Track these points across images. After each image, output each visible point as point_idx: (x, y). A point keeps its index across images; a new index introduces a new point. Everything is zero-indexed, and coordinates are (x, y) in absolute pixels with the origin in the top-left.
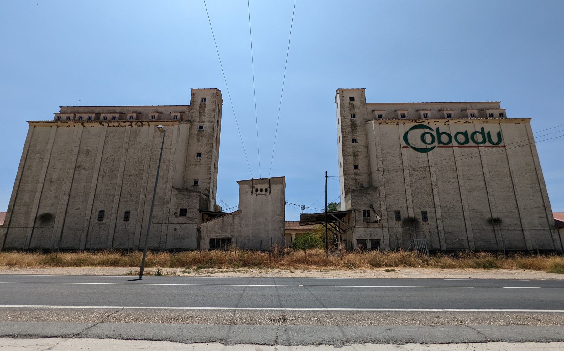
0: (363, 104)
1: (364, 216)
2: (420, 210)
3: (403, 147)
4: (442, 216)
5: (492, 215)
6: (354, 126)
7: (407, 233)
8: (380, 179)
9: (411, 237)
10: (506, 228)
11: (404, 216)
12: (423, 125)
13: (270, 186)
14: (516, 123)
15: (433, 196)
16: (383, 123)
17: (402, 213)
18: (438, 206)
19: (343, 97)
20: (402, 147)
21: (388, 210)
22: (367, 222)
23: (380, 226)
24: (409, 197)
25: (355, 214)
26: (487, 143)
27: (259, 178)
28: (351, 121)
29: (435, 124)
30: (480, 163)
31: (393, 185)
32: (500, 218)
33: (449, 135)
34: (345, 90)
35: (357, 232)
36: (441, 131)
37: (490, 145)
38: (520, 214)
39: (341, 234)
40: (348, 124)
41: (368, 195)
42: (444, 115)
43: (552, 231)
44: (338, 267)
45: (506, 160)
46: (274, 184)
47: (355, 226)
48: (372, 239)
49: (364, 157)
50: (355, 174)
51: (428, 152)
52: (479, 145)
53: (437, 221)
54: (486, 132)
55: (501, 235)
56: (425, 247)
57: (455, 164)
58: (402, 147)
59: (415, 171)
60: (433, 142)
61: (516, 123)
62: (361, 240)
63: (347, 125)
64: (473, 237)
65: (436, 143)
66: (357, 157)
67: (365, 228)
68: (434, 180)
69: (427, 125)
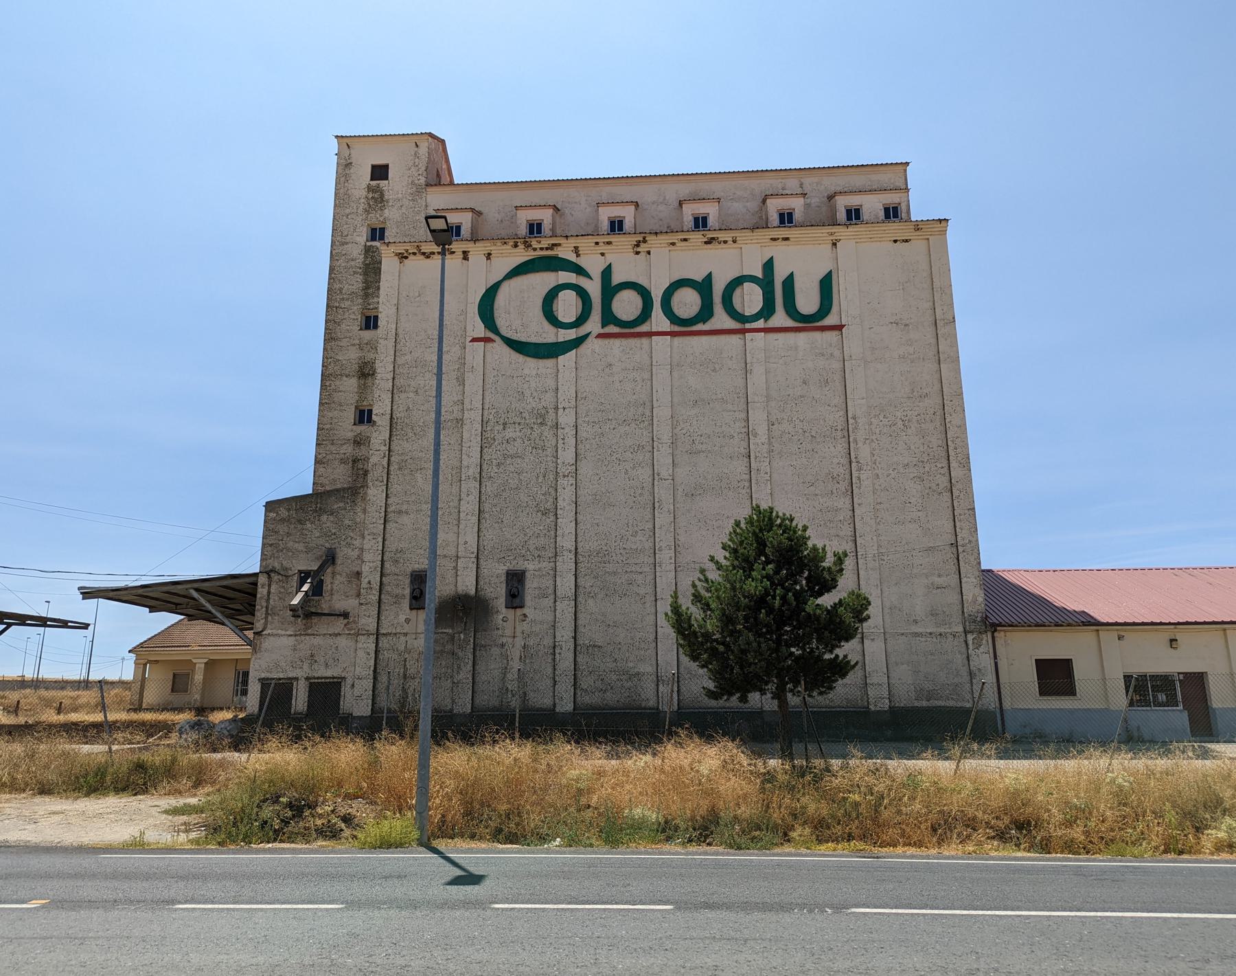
2: (502, 569)
7: (442, 652)
11: (441, 588)
12: (556, 258)
14: (895, 241)
16: (414, 254)
25: (269, 586)
28: (368, 250)
29: (603, 254)
31: (420, 480)
33: (645, 293)
40: (353, 263)
41: (324, 518)
43: (970, 637)
47: (262, 631)
48: (316, 676)
50: (355, 441)
61: (895, 241)
65: (594, 325)
67: (298, 638)
69: (572, 257)
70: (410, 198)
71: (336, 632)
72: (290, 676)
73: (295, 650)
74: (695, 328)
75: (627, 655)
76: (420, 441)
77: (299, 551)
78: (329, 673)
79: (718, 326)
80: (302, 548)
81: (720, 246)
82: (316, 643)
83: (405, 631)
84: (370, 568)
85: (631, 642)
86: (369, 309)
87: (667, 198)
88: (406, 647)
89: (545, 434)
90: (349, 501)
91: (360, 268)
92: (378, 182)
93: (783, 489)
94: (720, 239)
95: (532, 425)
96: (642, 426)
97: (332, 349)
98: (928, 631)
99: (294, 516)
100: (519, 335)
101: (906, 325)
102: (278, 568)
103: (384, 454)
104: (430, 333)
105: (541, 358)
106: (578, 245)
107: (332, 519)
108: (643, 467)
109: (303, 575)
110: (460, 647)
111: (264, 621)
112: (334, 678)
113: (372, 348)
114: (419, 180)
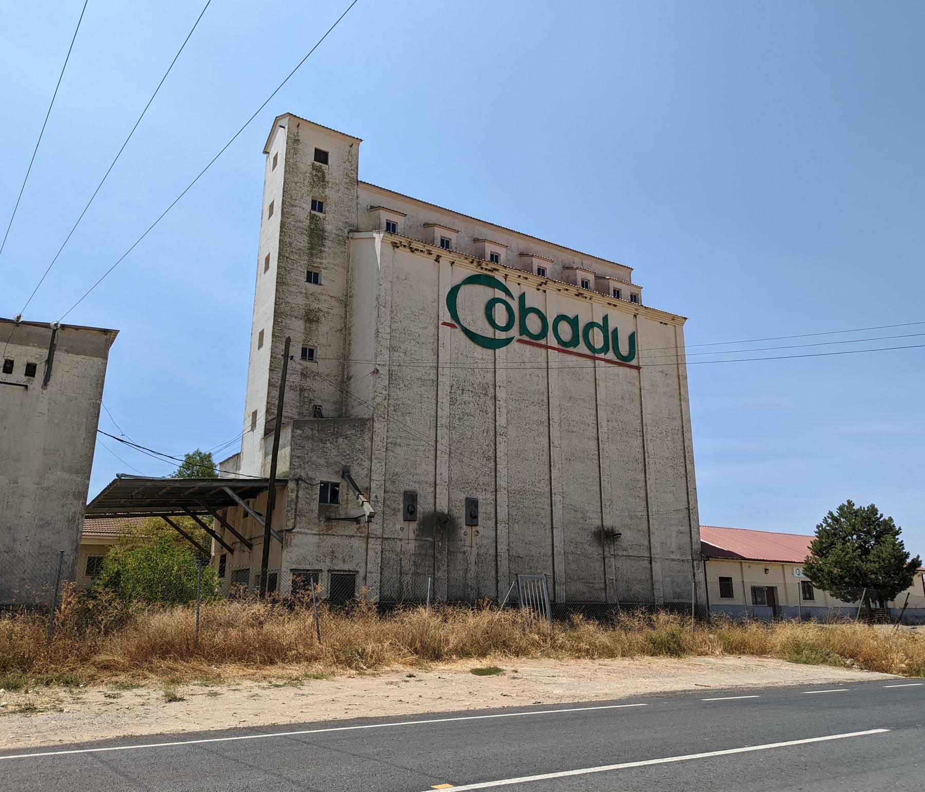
0: (348, 180)
1: (323, 499)
2: (463, 496)
3: (444, 324)
4: (509, 514)
5: (602, 522)
6: (316, 234)
7: (426, 555)
8: (378, 400)
9: (436, 566)
10: (625, 553)
11: (424, 507)
12: (493, 278)
13: (51, 355)
14: (661, 323)
15: (496, 461)
16: (405, 246)
17: (420, 500)
18: (502, 489)
19: (297, 141)
20: (441, 322)
21: (390, 487)
22: (329, 519)
23: (361, 533)
24: (443, 458)
25: (298, 491)
26: (611, 355)
27: (12, 317)
28: (312, 218)
29: (519, 284)
30: (594, 397)
31: (408, 421)
32: (617, 529)
33: (543, 318)
34: (306, 123)
35: (296, 545)
36: (528, 304)
37: (614, 358)
38: (650, 523)
39: (225, 551)
40: (300, 224)
41: (340, 440)
42: (532, 267)
43: (695, 563)
44: (318, 667)
45: (638, 398)
46: (67, 351)
47: (293, 529)
48: (336, 569)
49: (335, 329)
50: (302, 374)
51: (497, 350)
52: (596, 355)
53: (496, 527)
54: (611, 328)
55: (614, 568)
56: (543, 595)
57: (547, 390)
58: (441, 322)
59: (463, 390)
60: (508, 327)
61: (661, 323)
62: (304, 570)
63: (299, 227)
64: (564, 571)
65: (514, 332)
66: (314, 326)
67: (321, 537)
68: (502, 420)
69: (503, 281)
70: (346, 186)
71: (351, 534)
72: (316, 568)
73: (319, 547)
74: (569, 349)
75: (537, 564)
76: (408, 391)
77: (321, 466)
78: (346, 568)
79: (581, 351)
80: (324, 463)
81: (583, 299)
82: (335, 542)
83: (400, 537)
84: (377, 485)
85: (538, 555)
86: (313, 266)
87: (512, 247)
88: (401, 550)
89: (488, 402)
90: (359, 430)
91: (306, 230)
92: (321, 164)
93: (614, 463)
94: (584, 295)
95: (480, 395)
96: (542, 408)
97: (283, 292)
98: (678, 558)
99: (317, 435)
100: (471, 327)
101: (666, 375)
102: (304, 477)
103: (385, 397)
104: (414, 310)
105: (484, 347)
106: (508, 274)
107: (346, 442)
108: (543, 436)
109: (322, 485)
110: (439, 552)
111: (293, 520)
112: (350, 571)
113: (316, 299)
114: (352, 174)
